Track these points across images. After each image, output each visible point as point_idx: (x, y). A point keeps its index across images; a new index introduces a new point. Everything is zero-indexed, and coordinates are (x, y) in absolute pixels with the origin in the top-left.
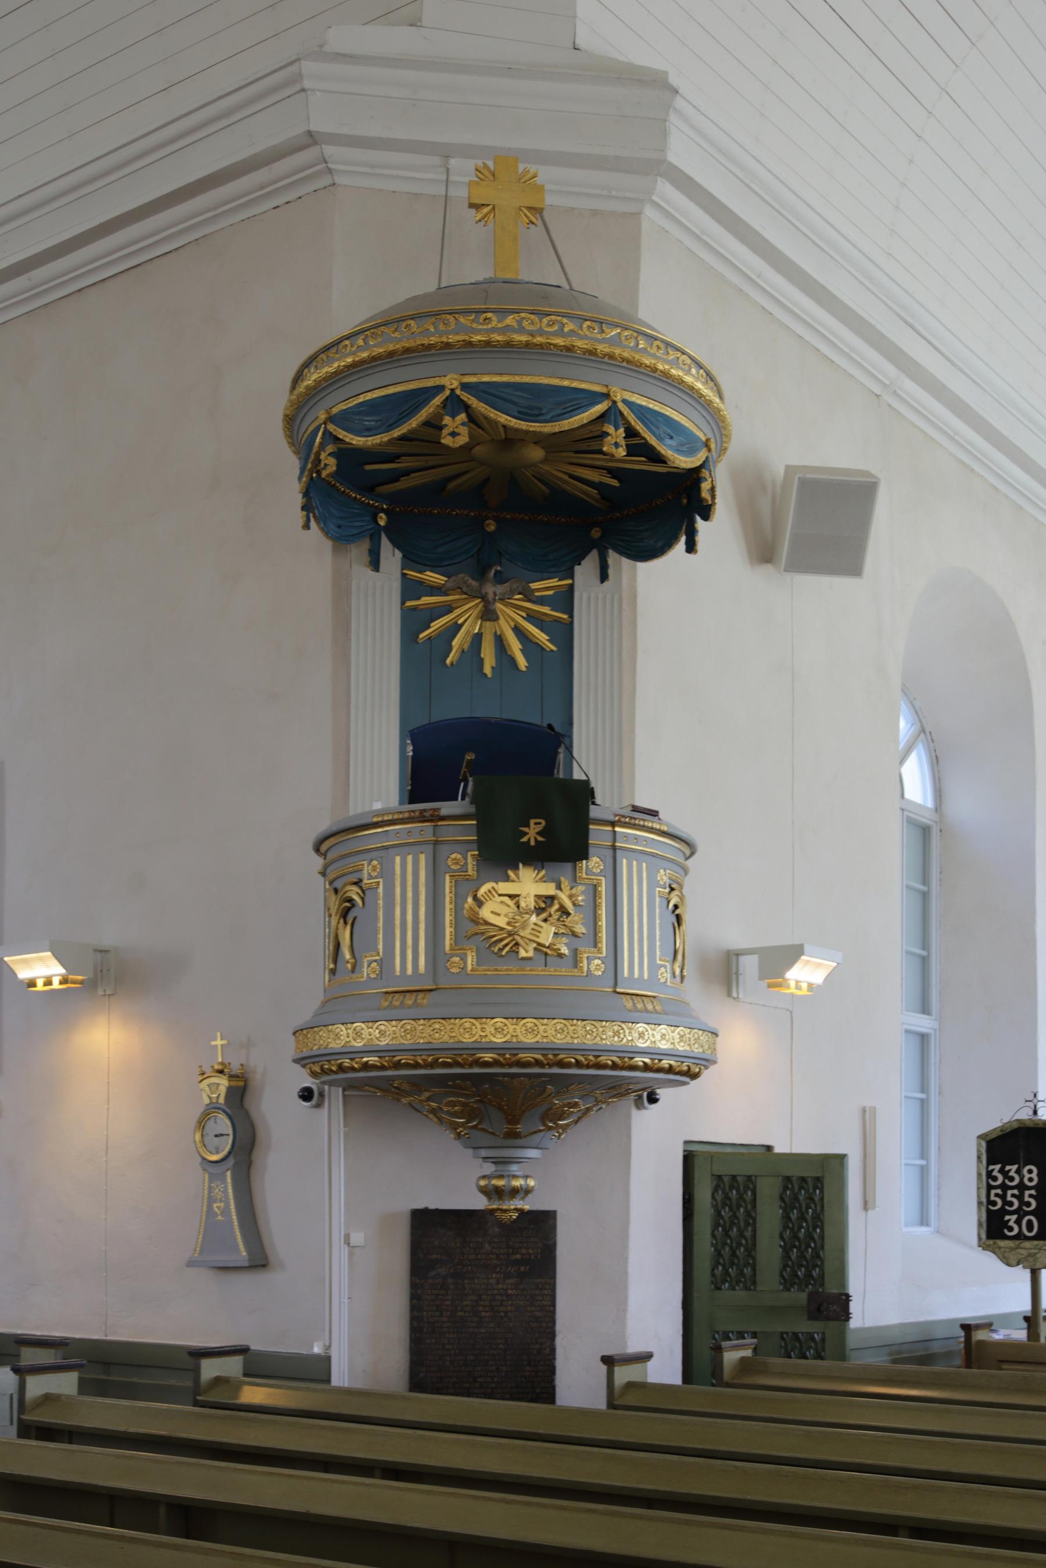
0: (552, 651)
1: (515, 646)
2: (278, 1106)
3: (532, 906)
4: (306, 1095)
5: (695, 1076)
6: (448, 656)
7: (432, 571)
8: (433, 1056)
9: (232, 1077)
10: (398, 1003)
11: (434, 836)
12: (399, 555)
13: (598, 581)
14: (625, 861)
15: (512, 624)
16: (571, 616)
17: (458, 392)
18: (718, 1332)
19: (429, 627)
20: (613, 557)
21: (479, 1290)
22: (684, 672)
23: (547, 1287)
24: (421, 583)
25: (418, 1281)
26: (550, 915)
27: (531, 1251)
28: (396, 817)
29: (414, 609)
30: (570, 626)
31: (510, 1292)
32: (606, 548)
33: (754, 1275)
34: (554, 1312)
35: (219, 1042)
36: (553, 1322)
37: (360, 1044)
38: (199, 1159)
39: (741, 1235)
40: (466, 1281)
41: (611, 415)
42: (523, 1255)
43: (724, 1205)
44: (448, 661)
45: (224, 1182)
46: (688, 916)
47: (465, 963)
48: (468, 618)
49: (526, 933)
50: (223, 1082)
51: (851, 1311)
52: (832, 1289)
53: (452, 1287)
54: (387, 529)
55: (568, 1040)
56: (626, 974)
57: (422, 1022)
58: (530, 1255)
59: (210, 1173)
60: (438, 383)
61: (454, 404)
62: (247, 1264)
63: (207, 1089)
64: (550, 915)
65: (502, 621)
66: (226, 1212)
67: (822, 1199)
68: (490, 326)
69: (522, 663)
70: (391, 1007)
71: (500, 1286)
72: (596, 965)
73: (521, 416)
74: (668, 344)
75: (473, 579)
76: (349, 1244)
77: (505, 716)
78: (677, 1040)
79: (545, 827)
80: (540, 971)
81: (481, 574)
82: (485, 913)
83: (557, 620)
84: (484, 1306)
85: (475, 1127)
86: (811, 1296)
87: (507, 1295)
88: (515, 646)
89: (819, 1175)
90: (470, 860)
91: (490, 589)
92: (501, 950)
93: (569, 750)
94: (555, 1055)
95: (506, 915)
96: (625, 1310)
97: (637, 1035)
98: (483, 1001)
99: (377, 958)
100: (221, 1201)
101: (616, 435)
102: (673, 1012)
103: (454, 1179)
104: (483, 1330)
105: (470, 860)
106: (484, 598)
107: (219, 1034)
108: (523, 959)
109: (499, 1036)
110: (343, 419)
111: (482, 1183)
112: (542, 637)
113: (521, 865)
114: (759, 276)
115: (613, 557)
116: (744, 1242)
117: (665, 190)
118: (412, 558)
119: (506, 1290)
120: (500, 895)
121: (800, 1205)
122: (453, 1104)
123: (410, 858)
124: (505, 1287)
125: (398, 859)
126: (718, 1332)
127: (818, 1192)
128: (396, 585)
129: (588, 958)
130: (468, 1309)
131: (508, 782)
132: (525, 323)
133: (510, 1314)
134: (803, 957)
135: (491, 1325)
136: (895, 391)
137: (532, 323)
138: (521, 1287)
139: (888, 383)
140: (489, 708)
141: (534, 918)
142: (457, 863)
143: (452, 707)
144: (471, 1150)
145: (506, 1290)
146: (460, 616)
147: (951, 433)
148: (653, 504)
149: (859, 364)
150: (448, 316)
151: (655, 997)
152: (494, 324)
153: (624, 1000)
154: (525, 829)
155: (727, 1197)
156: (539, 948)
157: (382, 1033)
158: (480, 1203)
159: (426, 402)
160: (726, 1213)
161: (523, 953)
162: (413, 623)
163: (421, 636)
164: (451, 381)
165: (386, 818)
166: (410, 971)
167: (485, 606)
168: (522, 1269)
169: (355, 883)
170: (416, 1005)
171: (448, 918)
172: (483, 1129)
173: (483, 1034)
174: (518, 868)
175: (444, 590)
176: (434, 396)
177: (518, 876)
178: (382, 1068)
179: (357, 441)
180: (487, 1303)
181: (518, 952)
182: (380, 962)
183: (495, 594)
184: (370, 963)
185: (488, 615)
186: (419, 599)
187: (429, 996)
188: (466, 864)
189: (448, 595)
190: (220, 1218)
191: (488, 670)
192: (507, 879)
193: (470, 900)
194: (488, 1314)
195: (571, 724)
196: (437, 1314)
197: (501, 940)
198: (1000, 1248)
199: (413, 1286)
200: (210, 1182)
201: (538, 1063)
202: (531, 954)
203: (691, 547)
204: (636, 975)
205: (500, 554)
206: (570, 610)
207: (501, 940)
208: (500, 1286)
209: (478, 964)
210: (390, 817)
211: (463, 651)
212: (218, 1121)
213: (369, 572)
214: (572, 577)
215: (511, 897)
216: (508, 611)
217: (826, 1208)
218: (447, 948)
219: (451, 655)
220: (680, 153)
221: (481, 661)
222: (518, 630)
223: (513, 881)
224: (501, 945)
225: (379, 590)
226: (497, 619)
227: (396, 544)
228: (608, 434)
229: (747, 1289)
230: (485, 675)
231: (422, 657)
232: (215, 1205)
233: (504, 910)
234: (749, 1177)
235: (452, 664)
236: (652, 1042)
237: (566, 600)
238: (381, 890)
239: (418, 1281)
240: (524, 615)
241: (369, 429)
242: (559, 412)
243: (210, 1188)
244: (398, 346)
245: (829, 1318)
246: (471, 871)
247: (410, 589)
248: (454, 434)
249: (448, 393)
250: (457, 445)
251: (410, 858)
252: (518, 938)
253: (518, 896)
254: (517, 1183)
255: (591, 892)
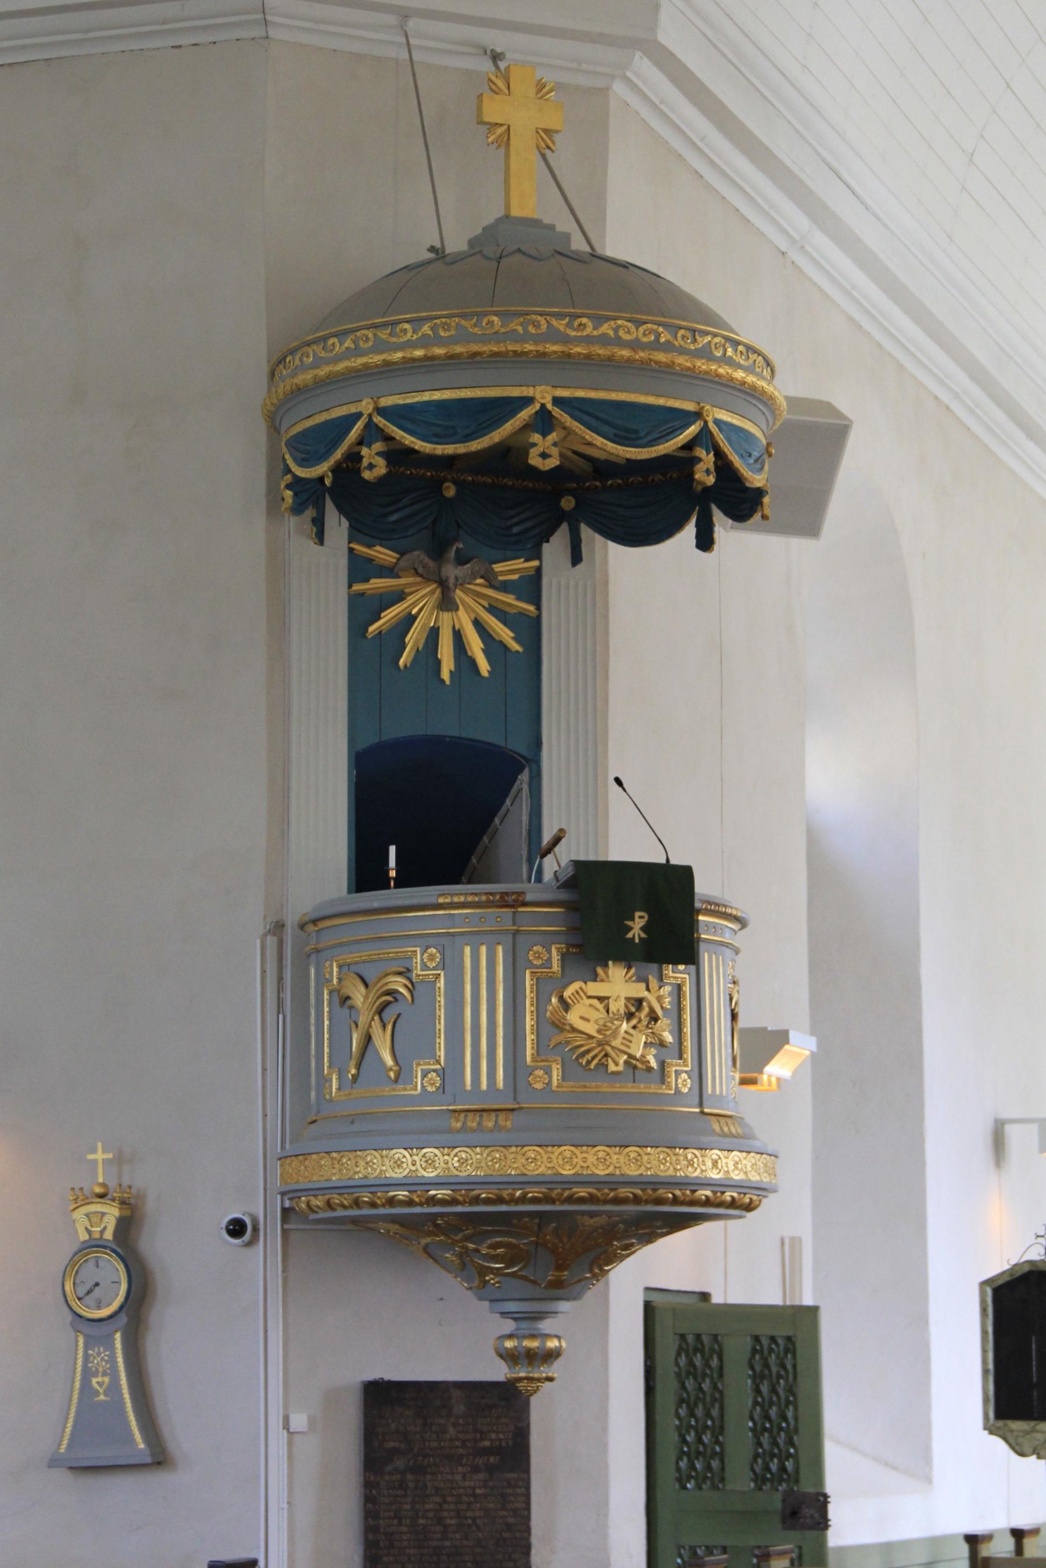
0: (517, 652)
1: (475, 645)
2: (186, 1247)
3: (622, 1010)
4: (236, 1228)
5: (749, 1207)
6: (401, 656)
7: (381, 546)
8: (501, 1188)
9: (123, 1203)
10: (490, 1124)
11: (514, 924)
12: (345, 523)
13: (569, 564)
14: (706, 955)
15: (473, 616)
16: (539, 608)
17: (549, 407)
18: (683, 1547)
19: (379, 618)
20: (586, 532)
21: (438, 1484)
22: (681, 696)
23: (521, 1484)
24: (370, 560)
25: (372, 1478)
26: (640, 1021)
27: (501, 1436)
28: (470, 899)
29: (362, 594)
30: (538, 619)
31: (478, 1491)
32: (579, 521)
33: (723, 1469)
34: (528, 1518)
35: (100, 1156)
36: (528, 1530)
37: (432, 1175)
38: (69, 1317)
39: (708, 1415)
40: (428, 1477)
41: (704, 438)
42: (491, 1440)
43: (688, 1373)
44: (401, 662)
45: (111, 1347)
46: (741, 1012)
47: (550, 1081)
48: (421, 602)
49: (617, 1043)
50: (112, 1213)
51: (830, 1516)
52: (807, 1487)
53: (411, 1485)
54: (331, 490)
55: (671, 1172)
56: (710, 1092)
57: (514, 1149)
58: (500, 1440)
59: (87, 1337)
60: (525, 394)
61: (544, 421)
62: (148, 1460)
63: (86, 1219)
64: (640, 1021)
65: (461, 612)
66: (114, 1388)
67: (794, 1366)
68: (585, 334)
69: (484, 666)
70: (464, 1129)
71: (467, 1483)
72: (685, 1083)
73: (617, 440)
74: (749, 348)
75: (430, 558)
76: (288, 1430)
77: (464, 735)
78: (731, 1167)
79: (648, 922)
80: (630, 1088)
81: (438, 553)
82: (573, 1017)
83: (522, 614)
84: (449, 1511)
85: (513, 1275)
86: (788, 1494)
87: (474, 1495)
88: (475, 645)
89: (790, 1334)
90: (554, 952)
91: (451, 571)
92: (589, 1062)
93: (536, 778)
94: (655, 1190)
95: (596, 1022)
96: (606, 1515)
97: (709, 1164)
98: (577, 1125)
99: (438, 1067)
100: (104, 1374)
101: (707, 459)
102: (739, 1139)
103: (449, 1339)
104: (448, 1543)
105: (554, 952)
106: (443, 584)
107: (100, 1145)
108: (614, 1073)
109: (568, 1167)
110: (399, 415)
111: (509, 1344)
112: (504, 634)
113: (610, 963)
114: (702, 139)
115: (586, 532)
116: (709, 1423)
117: (643, 66)
118: (359, 531)
119: (474, 1489)
120: (589, 997)
121: (771, 1375)
122: (495, 1246)
123: (483, 949)
124: (472, 1484)
125: (467, 950)
126: (683, 1547)
127: (789, 1356)
128: (343, 563)
129: (676, 1071)
130: (430, 1515)
131: (436, 804)
132: (621, 333)
133: (478, 1521)
134: (787, 1047)
135: (458, 1536)
136: (802, 247)
137: (629, 332)
138: (491, 1484)
139: (797, 237)
140: (448, 725)
141: (625, 1026)
142: (539, 957)
143: (405, 724)
144: (486, 1304)
145: (474, 1489)
146: (414, 605)
147: (849, 287)
148: (677, 485)
149: (828, 272)
150: (539, 318)
151: (730, 1117)
152: (589, 330)
153: (708, 1126)
154: (629, 923)
155: (691, 1363)
156: (631, 1064)
157: (463, 1162)
158: (498, 1372)
159: (513, 413)
160: (690, 1384)
161: (612, 1068)
162: (362, 611)
163: (371, 629)
164: (544, 395)
165: (456, 899)
166: (484, 1086)
167: (443, 593)
168: (492, 1460)
169: (400, 973)
170: (497, 1128)
171: (529, 1022)
172: (525, 1278)
173: (585, 1165)
174: (606, 965)
175: (395, 570)
176: (521, 408)
177: (607, 974)
178: (453, 1202)
179: (409, 440)
180: (452, 1507)
181: (607, 1066)
182: (442, 1073)
183: (457, 578)
184: (425, 1075)
185: (447, 604)
186: (367, 580)
187: (511, 1116)
188: (550, 958)
189: (399, 577)
190: (102, 1397)
191: (445, 675)
192: (595, 978)
193: (554, 1000)
194: (453, 1522)
195: (538, 744)
196: (396, 1522)
197: (588, 1051)
198: (1012, 1431)
199: (368, 1485)
200: (87, 1347)
201: (637, 1200)
202: (621, 1068)
203: (705, 541)
204: (718, 1092)
205: (459, 526)
206: (537, 602)
207: (588, 1051)
208: (467, 1483)
209: (564, 1079)
210: (462, 899)
211: (380, 632)
212: (101, 1263)
213: (318, 547)
214: (539, 557)
215: (601, 999)
216: (468, 600)
217: (799, 1378)
218: (529, 1059)
219: (405, 655)
220: (670, 34)
221: (438, 663)
222: (478, 624)
223: (602, 981)
224: (589, 1056)
225: (322, 564)
226: (457, 609)
227: (341, 510)
228: (700, 460)
229: (714, 1487)
230: (443, 681)
231: (372, 658)
232: (94, 1381)
233: (594, 1015)
234: (715, 1337)
235: (406, 666)
236: (702, 1171)
237: (531, 587)
238: (441, 984)
239: (372, 1478)
240: (486, 605)
241: (436, 435)
242: (656, 435)
243: (86, 1358)
244: (485, 349)
245: (804, 1527)
246: (556, 966)
247: (360, 569)
248: (544, 456)
249: (538, 406)
250: (547, 468)
251: (483, 949)
252: (608, 1049)
253: (608, 998)
254: (552, 1344)
255: (676, 992)
